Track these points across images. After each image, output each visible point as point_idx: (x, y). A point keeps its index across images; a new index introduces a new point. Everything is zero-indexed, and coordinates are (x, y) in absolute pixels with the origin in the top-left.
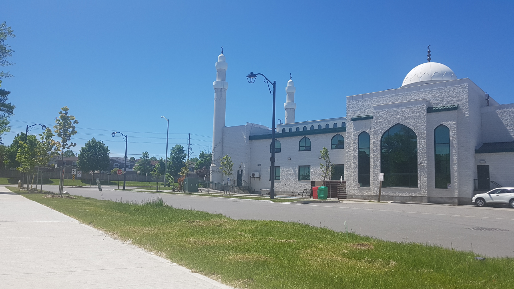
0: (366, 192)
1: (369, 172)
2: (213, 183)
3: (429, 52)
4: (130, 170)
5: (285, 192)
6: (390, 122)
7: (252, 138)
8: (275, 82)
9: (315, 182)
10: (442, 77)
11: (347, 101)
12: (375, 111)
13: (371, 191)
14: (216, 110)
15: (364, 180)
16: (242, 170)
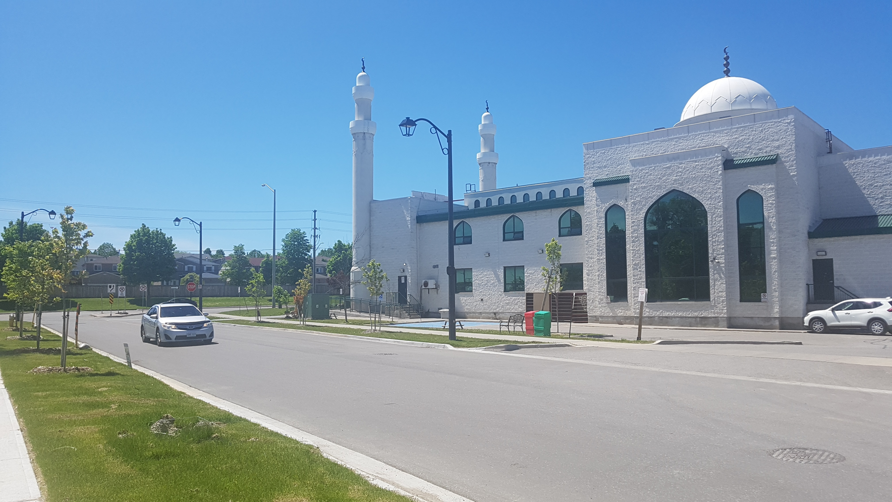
0: (620, 310)
1: (625, 276)
2: (356, 300)
3: (727, 59)
4: (214, 276)
5: (481, 313)
6: (659, 187)
7: (421, 219)
8: (450, 132)
9: (532, 294)
10: (751, 104)
11: (585, 151)
12: (633, 168)
13: (629, 310)
14: (357, 172)
15: (617, 289)
16: (406, 277)
